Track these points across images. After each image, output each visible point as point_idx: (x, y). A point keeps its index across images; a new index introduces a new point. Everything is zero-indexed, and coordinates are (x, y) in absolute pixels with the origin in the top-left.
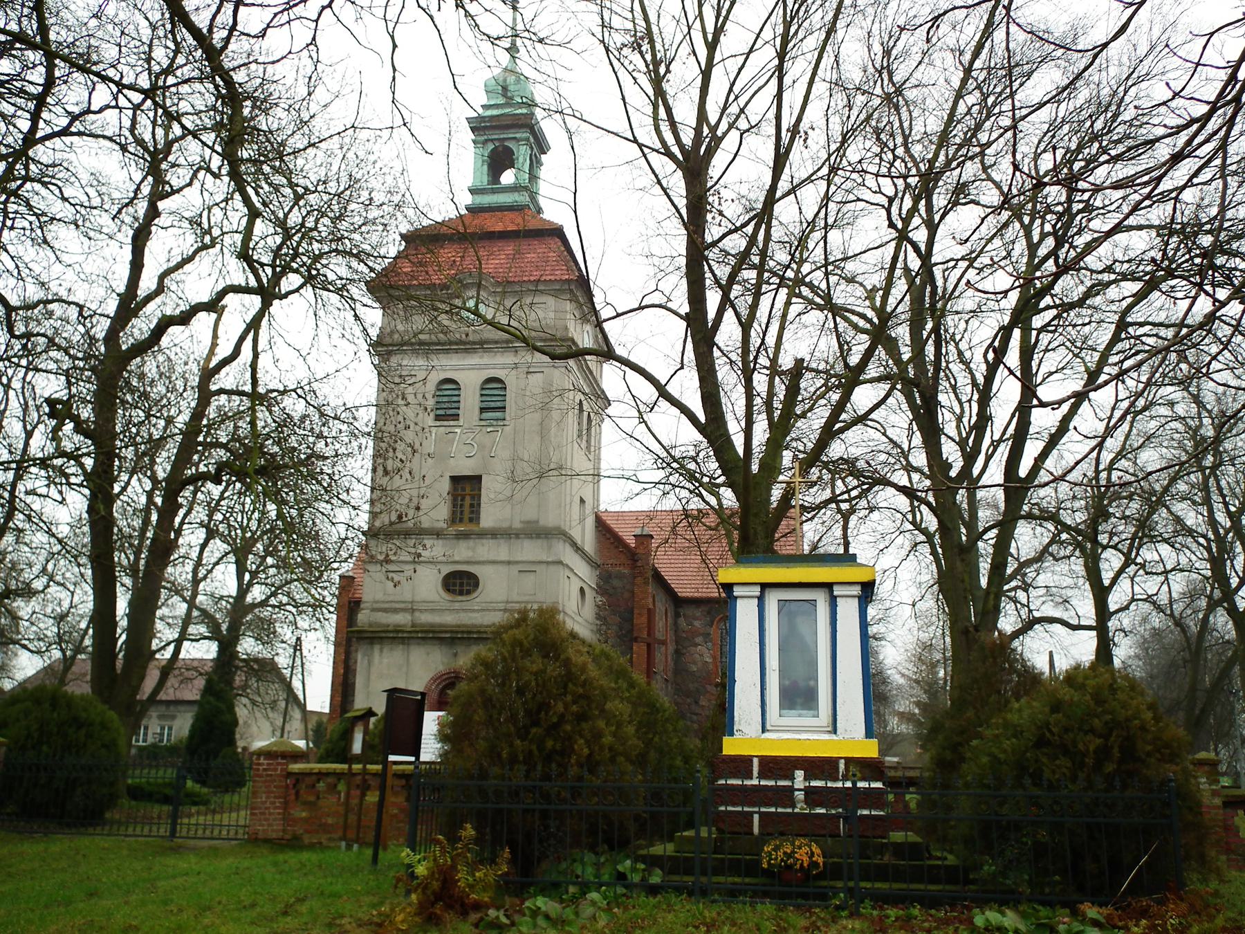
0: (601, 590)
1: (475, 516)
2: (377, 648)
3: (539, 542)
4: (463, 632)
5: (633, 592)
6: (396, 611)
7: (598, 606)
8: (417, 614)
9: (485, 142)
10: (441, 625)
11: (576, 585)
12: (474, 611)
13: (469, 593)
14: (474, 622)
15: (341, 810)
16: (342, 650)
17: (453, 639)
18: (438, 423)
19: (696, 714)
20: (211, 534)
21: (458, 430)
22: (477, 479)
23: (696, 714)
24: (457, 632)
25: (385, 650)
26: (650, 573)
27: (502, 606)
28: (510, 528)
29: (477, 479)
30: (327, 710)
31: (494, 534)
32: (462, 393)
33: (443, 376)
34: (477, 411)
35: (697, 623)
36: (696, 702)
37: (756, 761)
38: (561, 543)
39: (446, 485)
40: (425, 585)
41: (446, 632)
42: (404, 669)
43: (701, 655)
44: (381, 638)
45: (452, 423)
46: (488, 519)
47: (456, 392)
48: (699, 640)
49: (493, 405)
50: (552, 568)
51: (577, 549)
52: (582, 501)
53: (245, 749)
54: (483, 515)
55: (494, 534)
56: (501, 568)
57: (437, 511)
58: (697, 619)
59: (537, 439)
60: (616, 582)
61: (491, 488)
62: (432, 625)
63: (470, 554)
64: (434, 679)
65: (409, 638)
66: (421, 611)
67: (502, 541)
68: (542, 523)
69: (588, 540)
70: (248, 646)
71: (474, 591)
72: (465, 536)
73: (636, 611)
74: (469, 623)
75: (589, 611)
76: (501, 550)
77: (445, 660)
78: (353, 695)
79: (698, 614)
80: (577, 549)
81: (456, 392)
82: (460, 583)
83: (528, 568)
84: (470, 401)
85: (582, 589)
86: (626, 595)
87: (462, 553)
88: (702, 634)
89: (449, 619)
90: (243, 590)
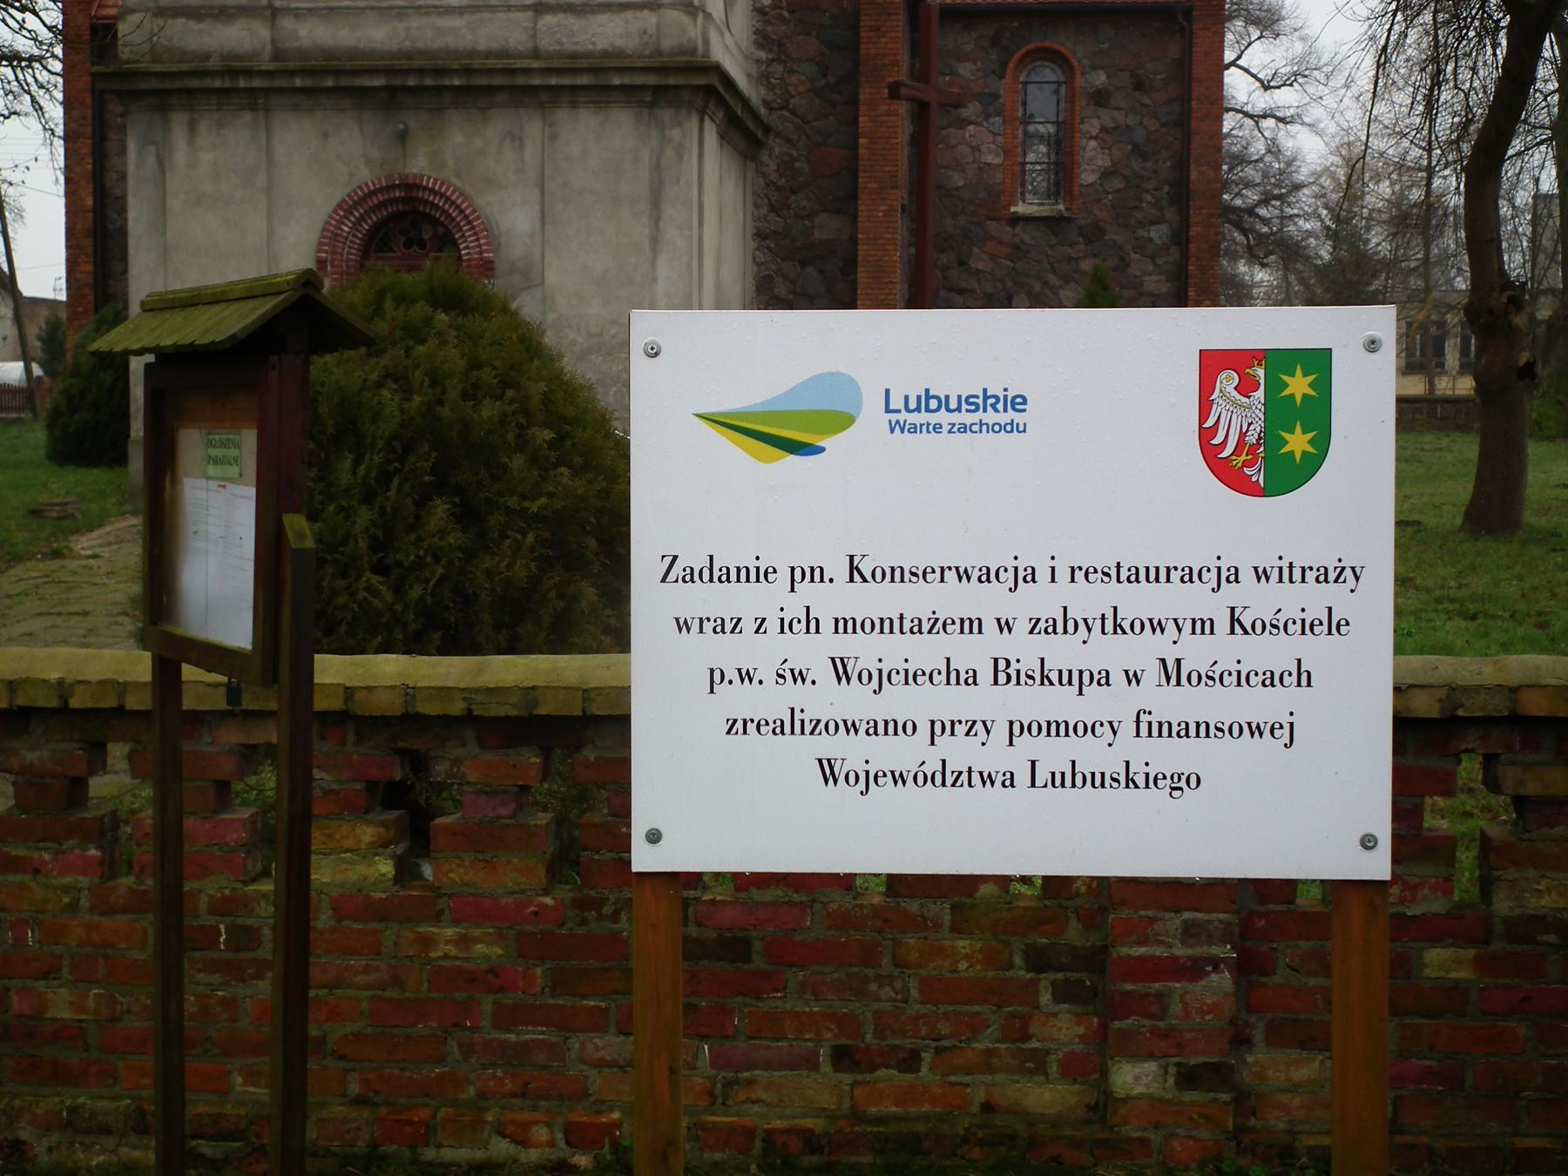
2: (179, 120)
4: (421, 72)
8: (286, 23)
10: (354, 54)
14: (451, 42)
15: (136, 938)
16: (85, 147)
17: (392, 91)
24: (405, 72)
25: (203, 127)
30: (63, 297)
36: (962, 263)
37: (137, 365)
41: (372, 72)
42: (261, 180)
43: (976, 149)
44: (190, 92)
58: (964, 58)
62: (331, 54)
66: (297, 14)
73: (866, 21)
74: (438, 44)
78: (124, 258)
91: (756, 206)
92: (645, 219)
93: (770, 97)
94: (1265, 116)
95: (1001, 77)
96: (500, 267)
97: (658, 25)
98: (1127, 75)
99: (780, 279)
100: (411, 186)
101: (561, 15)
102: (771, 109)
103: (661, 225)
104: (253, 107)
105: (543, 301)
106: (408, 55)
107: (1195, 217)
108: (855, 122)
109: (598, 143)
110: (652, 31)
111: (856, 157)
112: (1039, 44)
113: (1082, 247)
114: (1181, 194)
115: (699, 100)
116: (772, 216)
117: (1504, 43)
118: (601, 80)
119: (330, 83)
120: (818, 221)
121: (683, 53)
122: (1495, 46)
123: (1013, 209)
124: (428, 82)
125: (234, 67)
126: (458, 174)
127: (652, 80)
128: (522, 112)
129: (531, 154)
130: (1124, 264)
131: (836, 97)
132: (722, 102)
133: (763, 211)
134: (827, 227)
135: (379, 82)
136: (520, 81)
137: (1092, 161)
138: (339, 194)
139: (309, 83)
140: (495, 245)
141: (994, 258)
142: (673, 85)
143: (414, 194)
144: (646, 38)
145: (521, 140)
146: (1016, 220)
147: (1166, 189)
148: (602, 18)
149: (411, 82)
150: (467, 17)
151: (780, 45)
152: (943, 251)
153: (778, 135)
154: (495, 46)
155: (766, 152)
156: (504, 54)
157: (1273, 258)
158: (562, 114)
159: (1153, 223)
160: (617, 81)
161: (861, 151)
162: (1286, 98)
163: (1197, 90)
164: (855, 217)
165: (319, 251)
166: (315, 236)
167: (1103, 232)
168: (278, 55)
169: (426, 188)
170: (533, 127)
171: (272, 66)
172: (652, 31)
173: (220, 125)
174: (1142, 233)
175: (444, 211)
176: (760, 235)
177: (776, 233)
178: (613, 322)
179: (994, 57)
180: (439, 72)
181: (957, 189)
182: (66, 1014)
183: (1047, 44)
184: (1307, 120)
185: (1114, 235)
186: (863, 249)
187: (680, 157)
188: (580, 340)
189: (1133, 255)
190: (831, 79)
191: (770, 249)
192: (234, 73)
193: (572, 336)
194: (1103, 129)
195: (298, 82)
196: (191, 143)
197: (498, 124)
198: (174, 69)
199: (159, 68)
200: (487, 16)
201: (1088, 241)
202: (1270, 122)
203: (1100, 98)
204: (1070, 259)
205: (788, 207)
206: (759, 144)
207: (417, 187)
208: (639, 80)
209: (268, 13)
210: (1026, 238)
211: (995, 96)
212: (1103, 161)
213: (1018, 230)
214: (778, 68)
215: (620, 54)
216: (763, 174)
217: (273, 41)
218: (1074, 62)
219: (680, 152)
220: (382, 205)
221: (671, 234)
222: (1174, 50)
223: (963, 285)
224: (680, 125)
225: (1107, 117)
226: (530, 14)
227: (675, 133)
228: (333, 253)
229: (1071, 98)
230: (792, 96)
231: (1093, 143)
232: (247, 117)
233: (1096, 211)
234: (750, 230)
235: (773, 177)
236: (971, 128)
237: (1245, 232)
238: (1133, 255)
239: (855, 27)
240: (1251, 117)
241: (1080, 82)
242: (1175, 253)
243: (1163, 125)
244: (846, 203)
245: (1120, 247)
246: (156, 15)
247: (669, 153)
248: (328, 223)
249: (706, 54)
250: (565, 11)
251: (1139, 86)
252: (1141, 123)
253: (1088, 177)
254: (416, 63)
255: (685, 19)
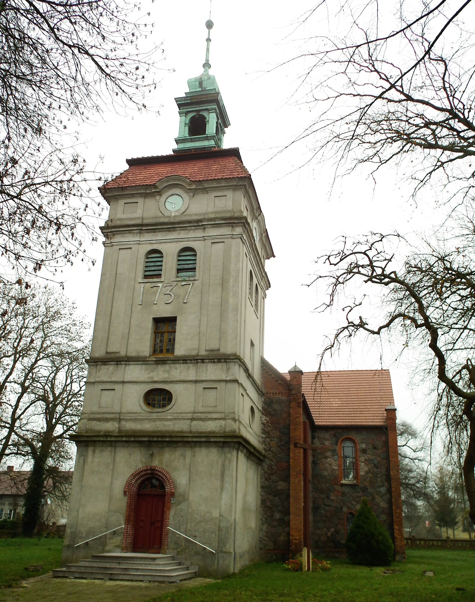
0: (265, 412)
1: (171, 350)
2: (91, 449)
3: (220, 365)
4: (158, 437)
5: (289, 414)
6: (107, 420)
7: (263, 424)
8: (123, 423)
9: (187, 113)
10: (141, 431)
11: (248, 404)
12: (168, 420)
13: (164, 406)
14: (167, 428)
17: (150, 442)
18: (146, 280)
19: (328, 506)
20: (25, 390)
21: (160, 285)
22: (172, 320)
23: (328, 506)
24: (153, 437)
25: (97, 451)
26: (302, 400)
27: (190, 416)
28: (198, 355)
29: (172, 320)
31: (185, 360)
32: (164, 259)
33: (150, 248)
34: (174, 271)
35: (327, 443)
36: (328, 497)
38: (237, 366)
39: (150, 324)
40: (131, 400)
41: (145, 436)
42: (111, 467)
44: (94, 441)
45: (156, 280)
46: (179, 350)
47: (160, 259)
48: (329, 454)
49: (186, 267)
50: (230, 385)
51: (249, 376)
52: (252, 344)
53: (54, 523)
54: (177, 346)
55: (185, 360)
56: (189, 386)
57: (143, 344)
58: (326, 439)
59: (219, 289)
60: (276, 406)
61: (182, 329)
63: (166, 375)
64: (134, 475)
65: (116, 441)
66: (126, 420)
67: (191, 365)
68: (222, 351)
69: (257, 374)
70: (50, 462)
71: (169, 404)
72: (162, 362)
73: (292, 427)
74: (164, 429)
75: (257, 426)
76: (190, 372)
77: (144, 460)
79: (328, 437)
80: (249, 376)
81: (160, 259)
82: (158, 398)
83: (211, 385)
84: (170, 264)
85: (252, 408)
86: (284, 415)
87: (160, 374)
88: (331, 450)
89: (147, 426)
90: (51, 427)
91: (261, 478)
92: (219, 481)
93: (266, 448)
94: (415, 459)
95: (337, 445)
96: (176, 495)
97: (225, 424)
98: (371, 445)
99: (268, 501)
100: (153, 470)
101: (198, 421)
102: (266, 451)
103: (224, 483)
104: (111, 446)
105: (188, 505)
106: (155, 432)
107: (393, 485)
108: (289, 455)
109: (207, 457)
110: (223, 426)
111: (289, 465)
112: (347, 436)
113: (361, 493)
114: (388, 478)
115: (237, 446)
116: (266, 482)
117: (469, 429)
118: (208, 440)
119: (133, 439)
120: (279, 483)
121: (232, 432)
122: (467, 430)
123: (341, 482)
124: (160, 439)
125: (107, 435)
126: (166, 466)
127: (222, 440)
128: (186, 448)
129: (187, 461)
130: (374, 498)
131: (284, 448)
132: (245, 447)
133: (264, 480)
134: (281, 485)
135: (146, 439)
136: (185, 439)
137: (363, 469)
138: (132, 471)
139: (127, 439)
140: (175, 488)
141: (336, 496)
142: (232, 441)
143: (153, 472)
144: (221, 428)
145: (185, 456)
146: (342, 485)
147: (384, 477)
148: (210, 422)
149: (155, 439)
150: (172, 421)
151: (269, 433)
152: (322, 494)
153: (268, 458)
154: (179, 430)
155: (264, 463)
156: (182, 432)
157: (422, 498)
158: (197, 449)
159: (381, 487)
160: (212, 440)
161: (291, 463)
162: (420, 454)
163: (391, 449)
164: (289, 483)
165: (125, 488)
166: (124, 484)
167: (367, 489)
168: (120, 431)
169: (157, 470)
170: (189, 453)
171: (118, 434)
172: (223, 426)
173: (102, 451)
174: (378, 489)
175: (162, 477)
176: (262, 487)
177: (267, 487)
178: (208, 512)
179: (334, 440)
180: (163, 437)
181: (326, 476)
182: (470, 519)
183: (349, 437)
184: (426, 460)
185: (370, 490)
186: (291, 492)
187: (230, 462)
188: (198, 517)
189: (376, 496)
190: (283, 443)
191: (265, 492)
192: (107, 436)
193: (196, 516)
194: (365, 460)
195: (124, 439)
196: (93, 456)
197: (179, 452)
198: (91, 435)
199: (87, 434)
200: (178, 421)
201: (363, 491)
202: (417, 461)
203: (364, 451)
204: (358, 497)
205: (270, 479)
206: (262, 461)
207: (155, 470)
208: (219, 440)
209: (118, 420)
210: (345, 490)
211: (335, 450)
212: (366, 469)
213: (343, 488)
214: (268, 440)
215: (214, 432)
216: (264, 470)
217: (119, 427)
218: (357, 442)
219: (230, 461)
220: (145, 475)
221: (227, 485)
222: (383, 438)
223: (328, 504)
224: (230, 453)
225: (366, 457)
226: (190, 421)
227: (229, 455)
228: (129, 489)
229: (356, 451)
230: (272, 447)
231: (363, 464)
232: (109, 449)
233: (365, 483)
234: (259, 485)
235: (266, 470)
236: (329, 459)
237: (413, 491)
238: (376, 496)
239: (289, 429)
240: (412, 459)
241: (358, 446)
242: (388, 496)
243: (382, 459)
244: (287, 479)
245: (372, 494)
246: (88, 420)
247: (227, 461)
248: (128, 480)
249: (239, 433)
250: (199, 420)
251: (374, 448)
252: (376, 458)
253: (362, 473)
254: (157, 434)
255: (233, 422)
